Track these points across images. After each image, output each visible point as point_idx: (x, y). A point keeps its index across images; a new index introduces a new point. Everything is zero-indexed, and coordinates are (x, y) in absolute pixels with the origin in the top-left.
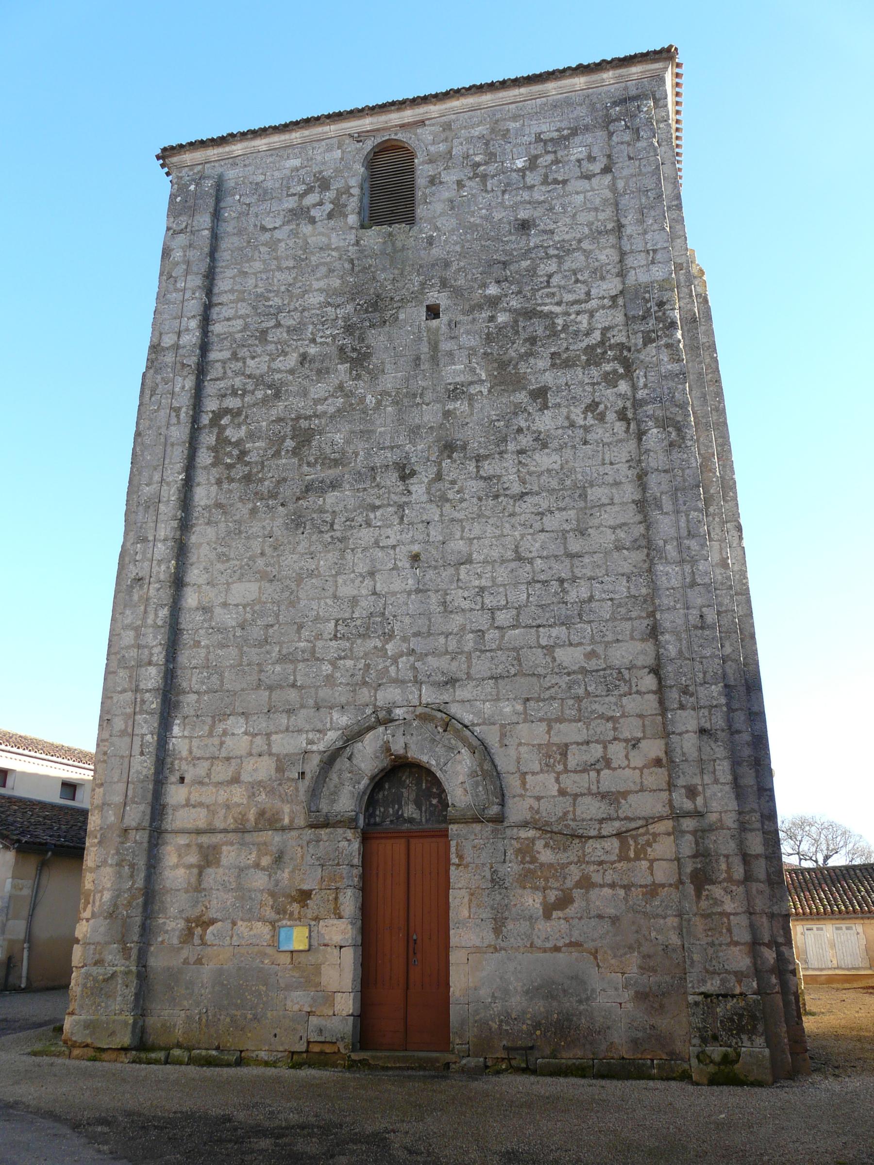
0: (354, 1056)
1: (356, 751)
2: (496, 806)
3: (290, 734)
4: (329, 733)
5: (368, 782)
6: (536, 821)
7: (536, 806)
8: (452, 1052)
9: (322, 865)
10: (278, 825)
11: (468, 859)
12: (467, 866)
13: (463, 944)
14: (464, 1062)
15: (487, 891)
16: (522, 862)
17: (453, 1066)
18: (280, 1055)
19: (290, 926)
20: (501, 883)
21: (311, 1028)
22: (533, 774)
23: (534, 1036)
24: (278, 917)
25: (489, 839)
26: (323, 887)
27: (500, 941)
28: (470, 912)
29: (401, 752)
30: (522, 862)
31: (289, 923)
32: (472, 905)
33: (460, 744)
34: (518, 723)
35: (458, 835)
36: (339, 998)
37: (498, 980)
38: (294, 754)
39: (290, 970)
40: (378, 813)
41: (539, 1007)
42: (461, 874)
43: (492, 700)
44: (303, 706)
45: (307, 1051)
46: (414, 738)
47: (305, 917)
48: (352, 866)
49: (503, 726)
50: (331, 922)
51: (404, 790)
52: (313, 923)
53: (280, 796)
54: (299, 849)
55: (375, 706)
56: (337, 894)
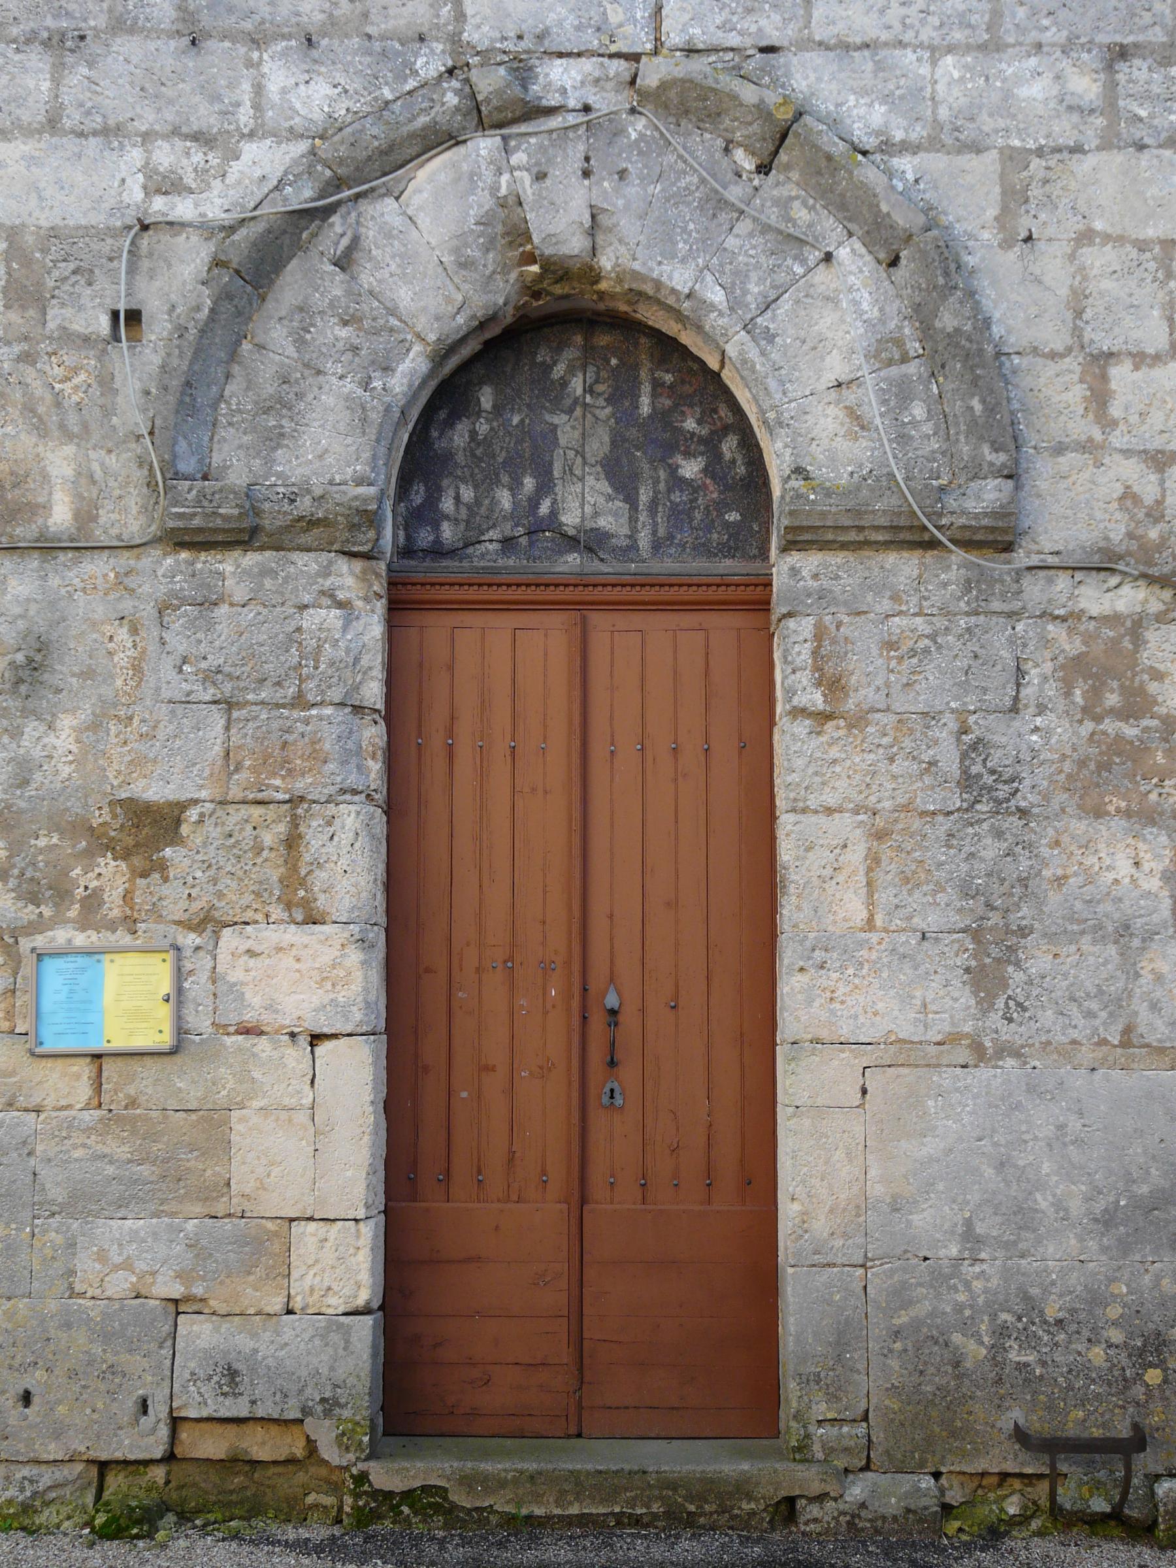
0: (384, 1476)
1: (370, 233)
2: (992, 483)
3: (71, 144)
4: (250, 150)
5: (424, 366)
6: (1147, 552)
7: (1148, 490)
8: (802, 1452)
9: (229, 705)
10: (24, 532)
11: (862, 695)
12: (857, 722)
13: (845, 1031)
14: (857, 1491)
15: (944, 825)
16: (1091, 712)
17: (815, 1511)
18: (47, 1477)
19: (89, 953)
20: (1003, 791)
21: (186, 1365)
22: (1140, 359)
23: (1138, 1391)
24: (29, 913)
25: (946, 612)
26: (235, 793)
27: (995, 1019)
28: (870, 903)
29: (574, 245)
30: (1091, 712)
31: (80, 939)
32: (879, 876)
33: (830, 227)
34: (1077, 149)
35: (822, 595)
36: (311, 1243)
37: (989, 1172)
38: (87, 231)
39: (88, 1131)
40: (447, 505)
41: (1158, 1279)
42: (834, 753)
43: (968, 48)
44: (121, 25)
45: (170, 1458)
46: (632, 190)
47: (155, 912)
48: (358, 709)
49: (1013, 158)
50: (272, 935)
51: (559, 419)
52: (190, 939)
53: (29, 409)
54: (123, 634)
55: (455, 40)
56: (295, 822)
